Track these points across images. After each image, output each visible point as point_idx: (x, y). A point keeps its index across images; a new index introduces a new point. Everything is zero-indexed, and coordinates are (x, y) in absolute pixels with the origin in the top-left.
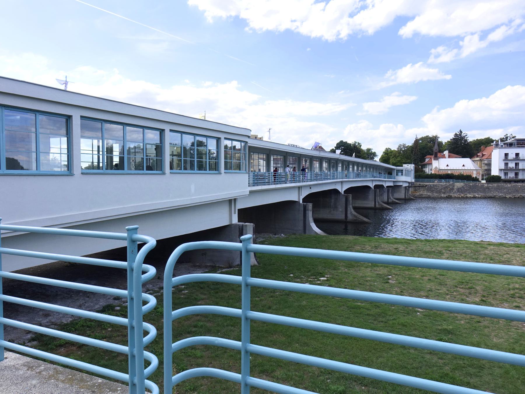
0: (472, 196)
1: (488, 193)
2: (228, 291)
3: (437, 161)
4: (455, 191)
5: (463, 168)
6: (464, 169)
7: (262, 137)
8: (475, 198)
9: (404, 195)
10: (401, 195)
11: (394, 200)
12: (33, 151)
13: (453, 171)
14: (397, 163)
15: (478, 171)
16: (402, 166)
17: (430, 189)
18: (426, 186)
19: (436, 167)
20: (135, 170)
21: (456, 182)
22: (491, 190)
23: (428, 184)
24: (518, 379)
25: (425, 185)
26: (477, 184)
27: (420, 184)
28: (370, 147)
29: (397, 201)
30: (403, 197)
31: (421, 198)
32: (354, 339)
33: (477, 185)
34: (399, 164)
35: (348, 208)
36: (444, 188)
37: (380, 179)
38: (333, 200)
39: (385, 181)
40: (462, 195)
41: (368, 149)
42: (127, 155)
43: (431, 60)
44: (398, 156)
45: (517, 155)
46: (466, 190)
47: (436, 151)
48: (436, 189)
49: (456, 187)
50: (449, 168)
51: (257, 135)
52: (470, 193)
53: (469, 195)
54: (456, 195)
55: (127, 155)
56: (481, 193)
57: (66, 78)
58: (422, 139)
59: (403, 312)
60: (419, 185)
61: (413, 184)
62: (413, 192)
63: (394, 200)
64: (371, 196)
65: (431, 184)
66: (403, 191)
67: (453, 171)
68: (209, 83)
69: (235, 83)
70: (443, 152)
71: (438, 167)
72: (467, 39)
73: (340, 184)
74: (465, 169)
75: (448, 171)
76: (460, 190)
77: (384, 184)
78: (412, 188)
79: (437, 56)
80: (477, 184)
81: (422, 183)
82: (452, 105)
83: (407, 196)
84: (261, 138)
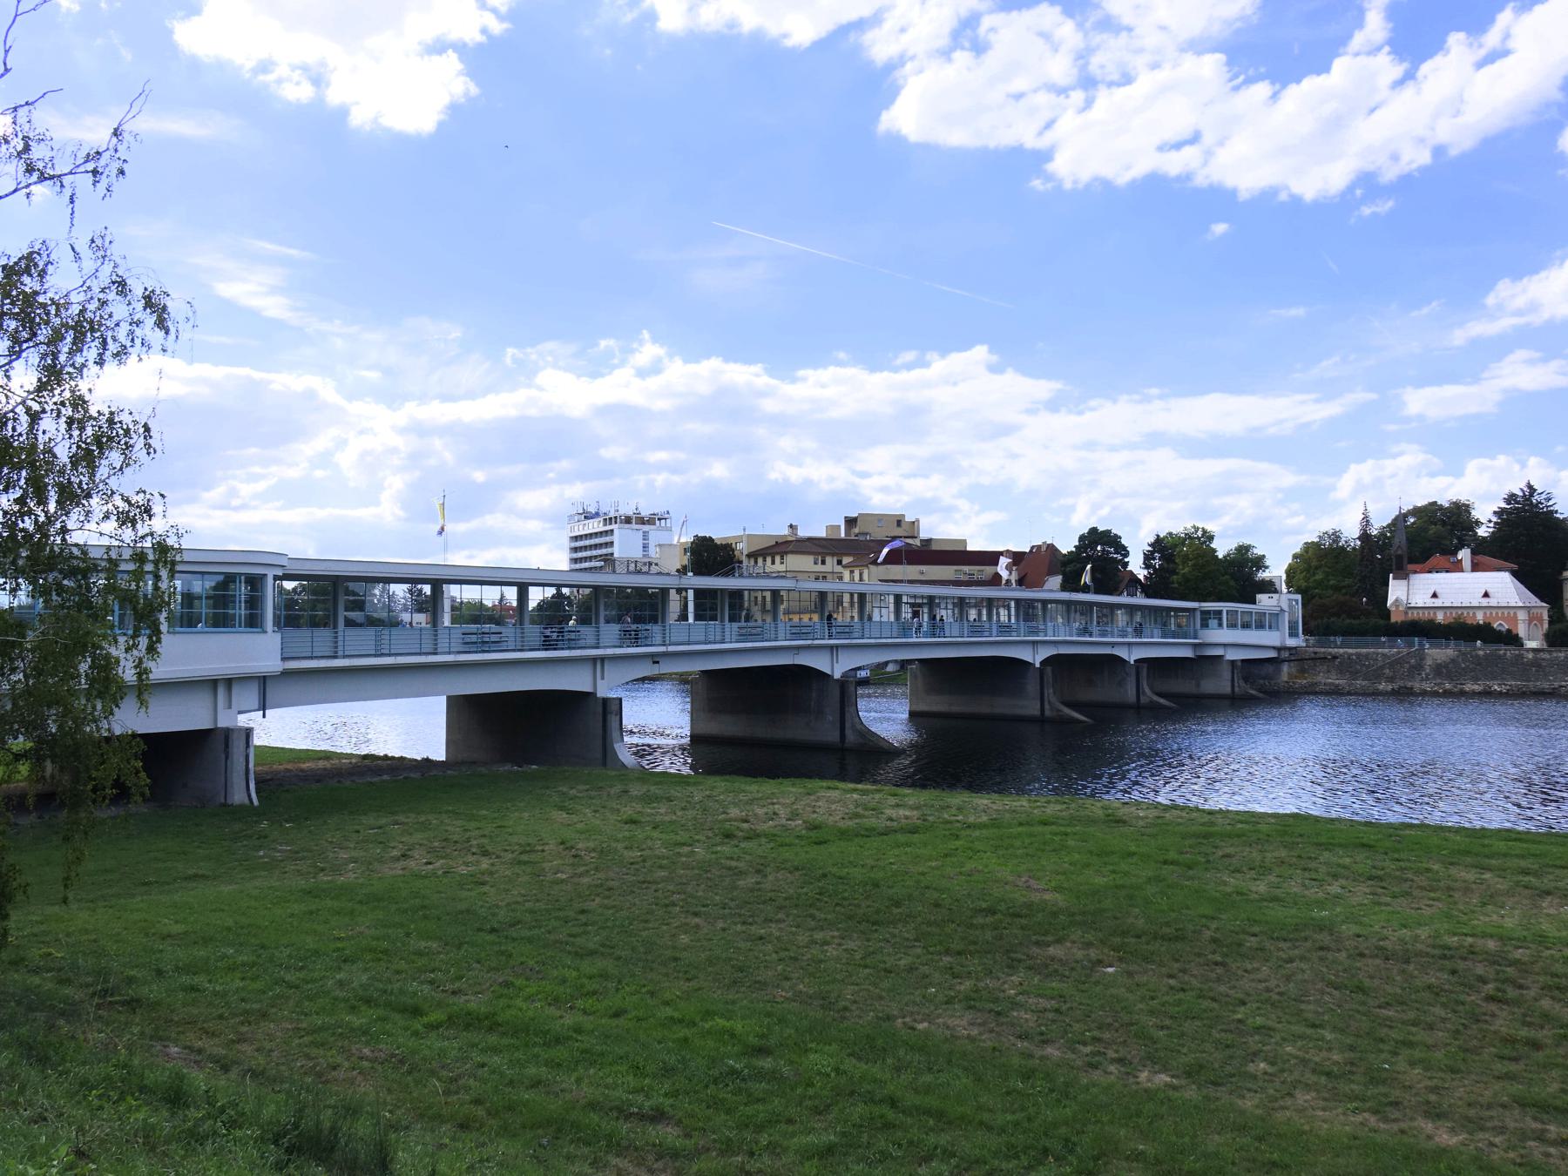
0: (1481, 688)
1: (1537, 680)
3: (1404, 582)
4: (1427, 675)
5: (1485, 602)
6: (1486, 605)
7: (918, 521)
8: (1487, 694)
9: (1229, 684)
10: (1221, 684)
11: (1156, 698)
13: (1418, 613)
15: (1535, 611)
16: (1254, 602)
17: (1347, 666)
18: (1335, 657)
19: (1397, 600)
20: (1062, 591)
22: (1547, 670)
23: (1341, 651)
24: (408, 935)
25: (1330, 654)
26: (1502, 652)
27: (1316, 653)
28: (1247, 542)
29: (1162, 701)
30: (1228, 690)
31: (1311, 692)
33: (1500, 657)
35: (847, 715)
36: (1392, 665)
37: (904, 640)
38: (814, 695)
39: (1129, 644)
40: (1448, 686)
41: (1240, 546)
44: (1316, 568)
46: (1463, 669)
47: (1399, 552)
48: (1368, 667)
49: (1429, 662)
50: (1437, 603)
51: (904, 516)
52: (1476, 680)
53: (1469, 687)
54: (1427, 686)
56: (1515, 679)
58: (1416, 511)
60: (1313, 655)
61: (1294, 652)
62: (1296, 677)
63: (1156, 698)
64: (1032, 687)
65: (1350, 651)
66: (1227, 675)
67: (1418, 613)
69: (980, 352)
70: (1455, 553)
71: (1404, 598)
74: (1491, 605)
75: (1435, 613)
76: (1444, 671)
77: (1122, 653)
78: (1292, 664)
80: (1502, 652)
81: (1323, 650)
83: (1239, 686)
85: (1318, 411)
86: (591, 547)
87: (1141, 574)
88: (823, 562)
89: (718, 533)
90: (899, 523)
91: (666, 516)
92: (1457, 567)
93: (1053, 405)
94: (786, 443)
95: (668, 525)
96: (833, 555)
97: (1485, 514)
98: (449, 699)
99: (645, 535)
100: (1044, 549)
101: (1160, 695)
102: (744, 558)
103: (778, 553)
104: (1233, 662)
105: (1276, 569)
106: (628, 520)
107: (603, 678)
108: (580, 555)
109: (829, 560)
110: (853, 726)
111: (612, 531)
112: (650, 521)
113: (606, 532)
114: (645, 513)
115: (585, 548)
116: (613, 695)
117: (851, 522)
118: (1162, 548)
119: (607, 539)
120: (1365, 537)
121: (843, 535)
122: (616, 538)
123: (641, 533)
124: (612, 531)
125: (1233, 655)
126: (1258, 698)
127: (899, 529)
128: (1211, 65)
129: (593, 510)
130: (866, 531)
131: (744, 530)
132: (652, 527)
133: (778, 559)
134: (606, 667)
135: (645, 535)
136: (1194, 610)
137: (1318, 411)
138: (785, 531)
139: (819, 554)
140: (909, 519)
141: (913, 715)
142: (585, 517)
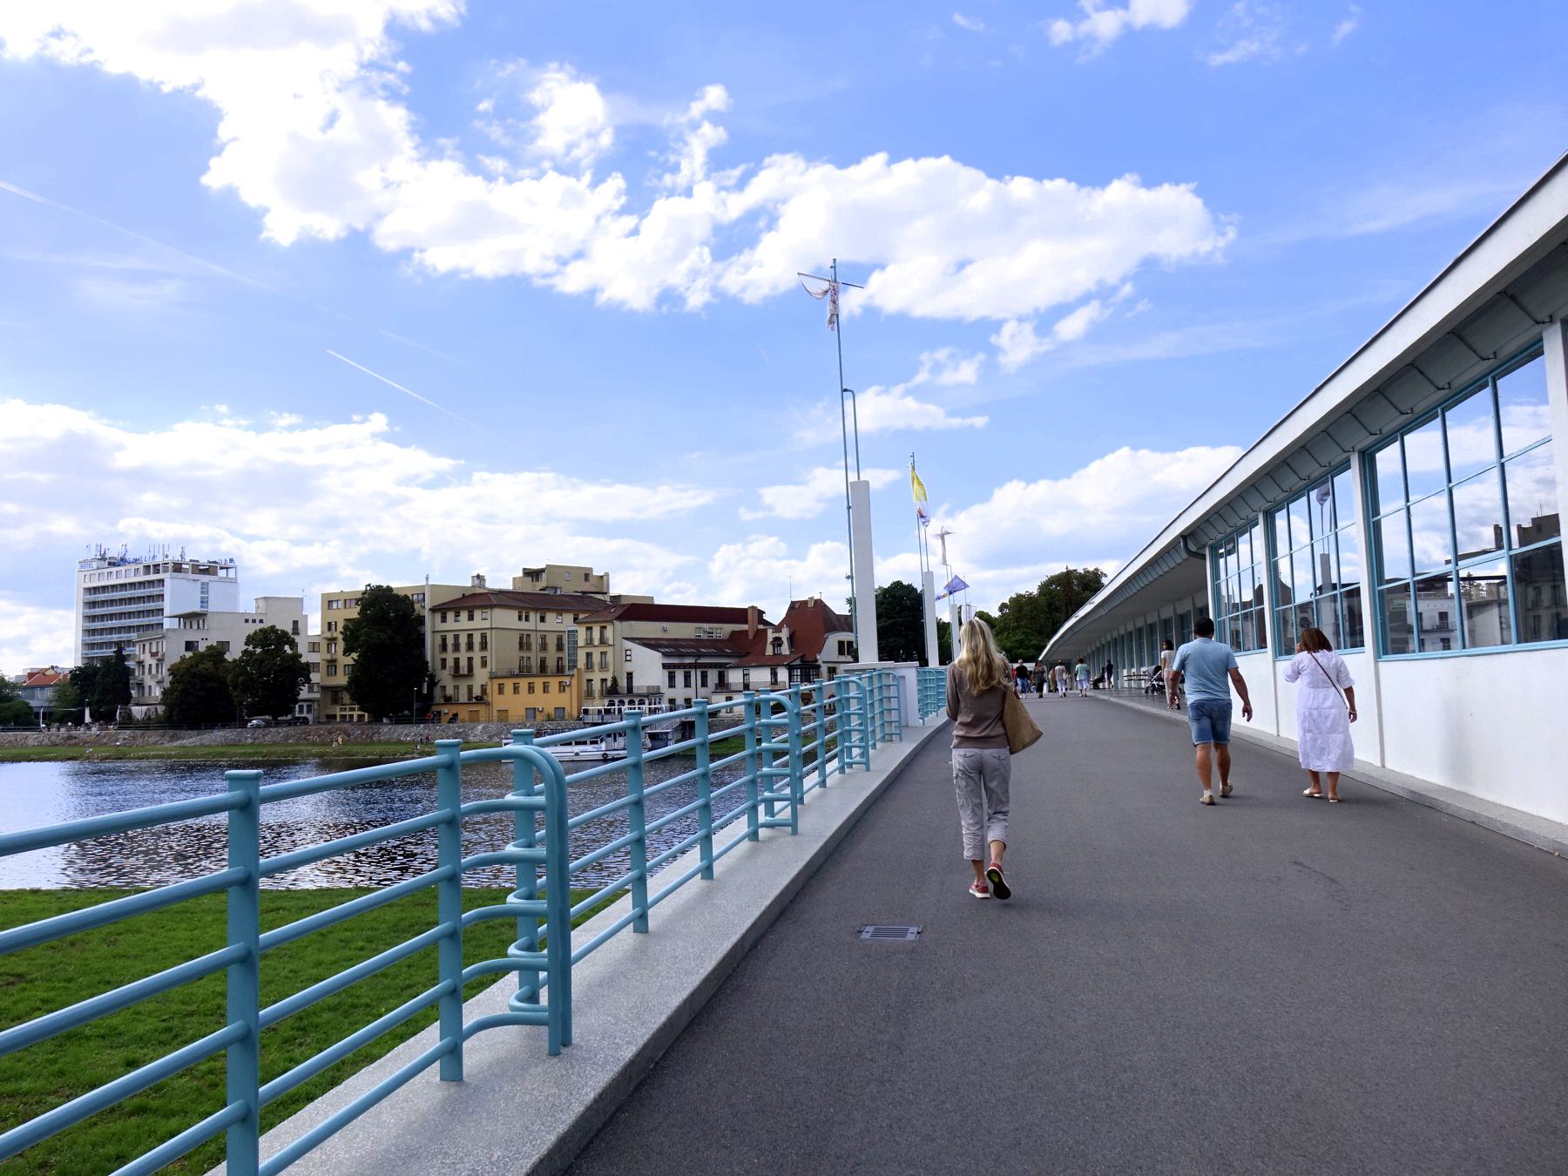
2: (337, 1074)
12: (851, 596)
14: (1015, 648)
34: (1021, 650)
42: (844, 654)
43: (922, 377)
51: (591, 569)
55: (844, 654)
68: (288, 419)
72: (1008, 329)
79: (937, 369)
82: (986, 497)
84: (602, 577)
85: (690, 499)
88: (543, 619)
91: (229, 564)
93: (438, 482)
94: (149, 499)
96: (536, 610)
99: (205, 588)
100: (811, 605)
102: (427, 613)
103: (464, 608)
106: (178, 568)
108: (98, 611)
109: (532, 615)
112: (210, 570)
115: (103, 603)
118: (797, 609)
119: (154, 591)
122: (167, 591)
123: (199, 584)
124: (161, 582)
127: (586, 583)
128: (360, 226)
130: (555, 584)
131: (427, 579)
132: (213, 578)
133: (477, 614)
135: (205, 588)
137: (690, 499)
138: (468, 583)
139: (524, 608)
140: (597, 572)
142: (110, 564)
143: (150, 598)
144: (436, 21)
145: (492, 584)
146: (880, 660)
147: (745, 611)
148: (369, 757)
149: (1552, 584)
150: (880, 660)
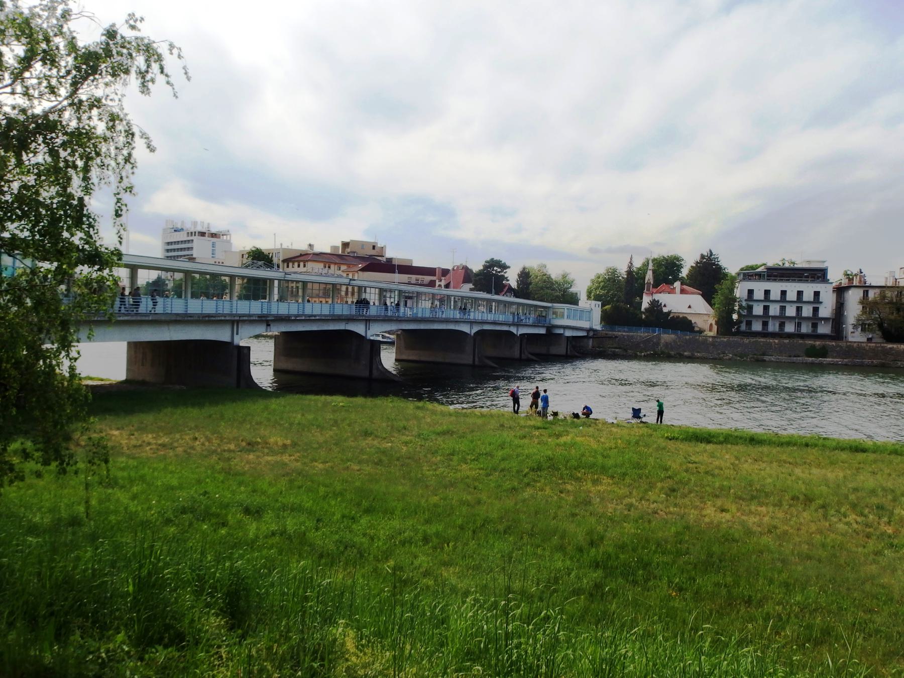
10: (561, 349)
11: (530, 356)
18: (616, 337)
21: (665, 333)
32: (119, 237)
45: (817, 294)
49: (662, 341)
57: (186, 73)
59: (118, 299)
63: (530, 356)
66: (564, 344)
73: (364, 322)
86: (178, 250)
87: (55, 264)
89: (265, 245)
90: (374, 247)
92: (672, 291)
95: (228, 238)
97: (689, 262)
98: (129, 343)
99: (213, 245)
101: (532, 354)
103: (302, 261)
104: (568, 337)
105: (581, 288)
106: (202, 234)
107: (237, 334)
109: (332, 266)
110: (378, 368)
111: (192, 240)
113: (189, 241)
114: (213, 231)
115: (174, 250)
116: (242, 344)
117: (345, 245)
120: (630, 273)
121: (340, 252)
124: (192, 240)
125: (568, 333)
126: (495, 368)
129: (179, 227)
134: (240, 326)
135: (213, 245)
136: (549, 307)
141: (396, 360)
143: (171, 250)
144: (714, 298)
145: (318, 249)
146: (249, 348)
147: (435, 269)
148: (479, 392)
149: (358, 546)
150: (249, 348)
